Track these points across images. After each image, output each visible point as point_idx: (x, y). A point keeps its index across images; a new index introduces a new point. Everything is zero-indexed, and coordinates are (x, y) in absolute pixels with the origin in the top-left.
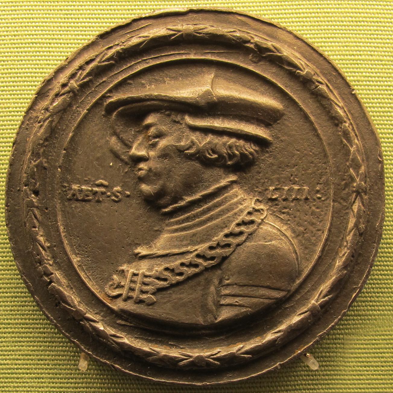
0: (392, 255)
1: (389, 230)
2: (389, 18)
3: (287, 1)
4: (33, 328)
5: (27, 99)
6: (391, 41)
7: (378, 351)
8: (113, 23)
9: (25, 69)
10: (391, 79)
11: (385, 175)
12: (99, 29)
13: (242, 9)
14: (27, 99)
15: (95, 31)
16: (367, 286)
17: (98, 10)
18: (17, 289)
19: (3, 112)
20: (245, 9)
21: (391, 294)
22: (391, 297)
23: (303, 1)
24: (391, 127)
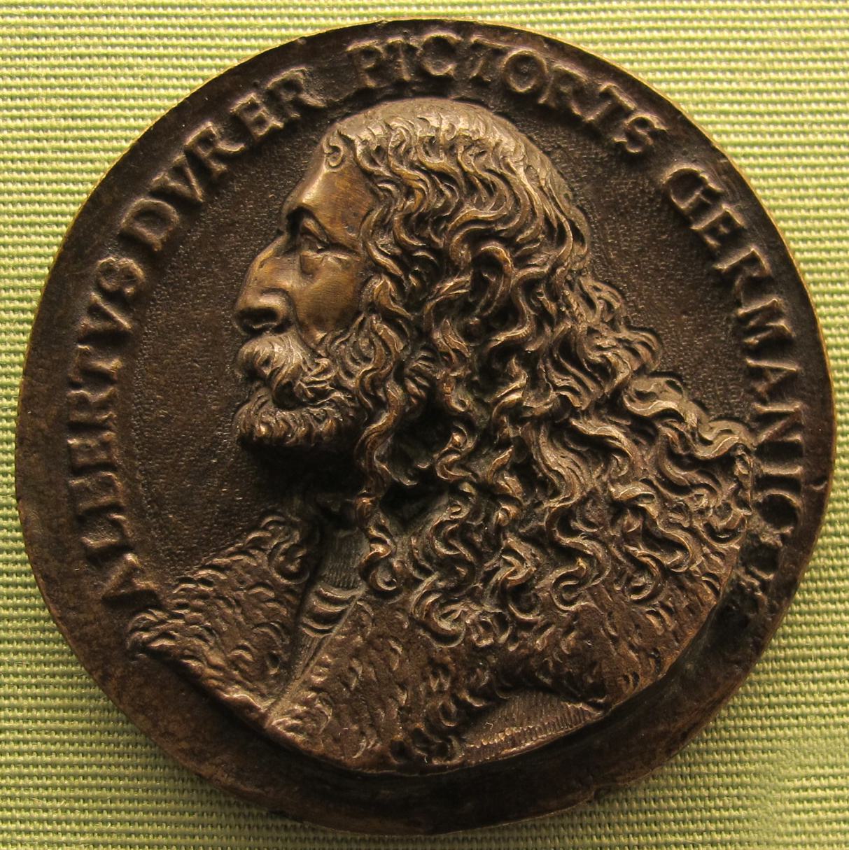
0: (846, 640)
1: (840, 657)
2: (807, 647)
3: (538, 3)
4: (44, 653)
5: (63, 214)
6: (845, 696)
7: (24, 747)
8: (252, 48)
9: (711, 29)
10: (843, 275)
11: (830, 353)
12: (218, 62)
13: (506, 18)
14: (63, 214)
15: (210, 68)
16: (795, 608)
17: (189, 16)
18: (52, 644)
19: (7, 67)
20: (515, 18)
21: (845, 504)
22: (843, 623)
23: (594, 3)
24: (844, 223)
